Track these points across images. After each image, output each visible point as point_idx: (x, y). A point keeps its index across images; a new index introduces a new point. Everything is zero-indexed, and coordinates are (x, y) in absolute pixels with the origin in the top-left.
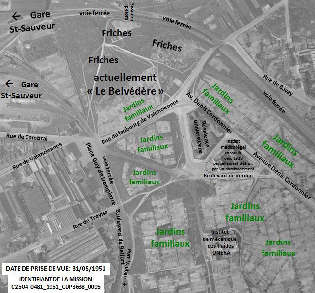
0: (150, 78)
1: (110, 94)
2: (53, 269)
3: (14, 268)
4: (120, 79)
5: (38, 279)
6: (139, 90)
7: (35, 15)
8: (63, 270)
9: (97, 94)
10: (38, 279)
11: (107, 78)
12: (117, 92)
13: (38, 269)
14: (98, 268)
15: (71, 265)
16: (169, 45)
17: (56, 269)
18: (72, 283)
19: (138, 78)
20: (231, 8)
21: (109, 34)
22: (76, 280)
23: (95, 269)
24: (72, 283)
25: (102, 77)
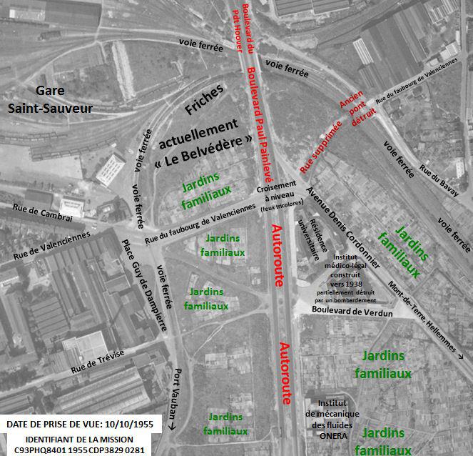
0: (229, 125)
1: (184, 160)
2: (77, 424)
3: (19, 423)
4: (192, 138)
5: (54, 439)
6: (220, 145)
7: (43, 91)
8: (92, 425)
9: (168, 165)
10: (54, 439)
11: (176, 141)
12: (193, 155)
13: (54, 425)
14: (142, 424)
15: (102, 418)
16: (205, 97)
17: (81, 424)
18: (104, 445)
19: (214, 130)
20: (379, 57)
21: (196, 106)
22: (111, 440)
23: (138, 425)
24: (104, 445)
25: (169, 142)
